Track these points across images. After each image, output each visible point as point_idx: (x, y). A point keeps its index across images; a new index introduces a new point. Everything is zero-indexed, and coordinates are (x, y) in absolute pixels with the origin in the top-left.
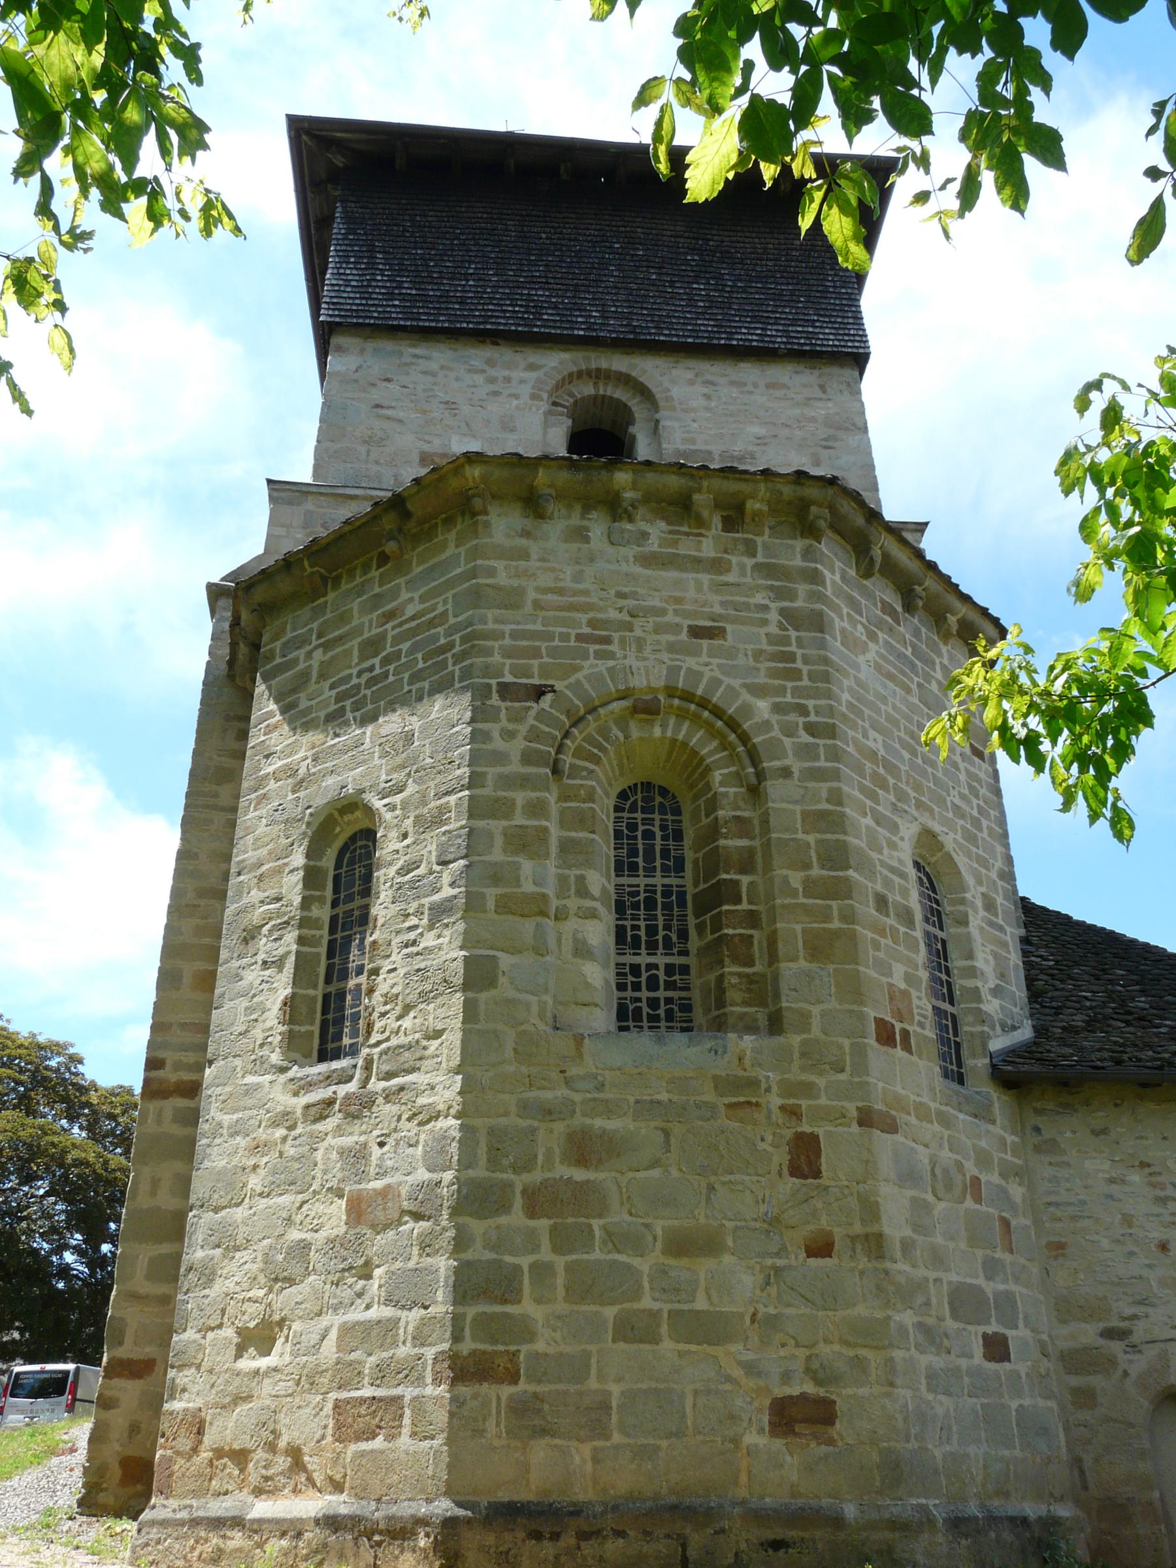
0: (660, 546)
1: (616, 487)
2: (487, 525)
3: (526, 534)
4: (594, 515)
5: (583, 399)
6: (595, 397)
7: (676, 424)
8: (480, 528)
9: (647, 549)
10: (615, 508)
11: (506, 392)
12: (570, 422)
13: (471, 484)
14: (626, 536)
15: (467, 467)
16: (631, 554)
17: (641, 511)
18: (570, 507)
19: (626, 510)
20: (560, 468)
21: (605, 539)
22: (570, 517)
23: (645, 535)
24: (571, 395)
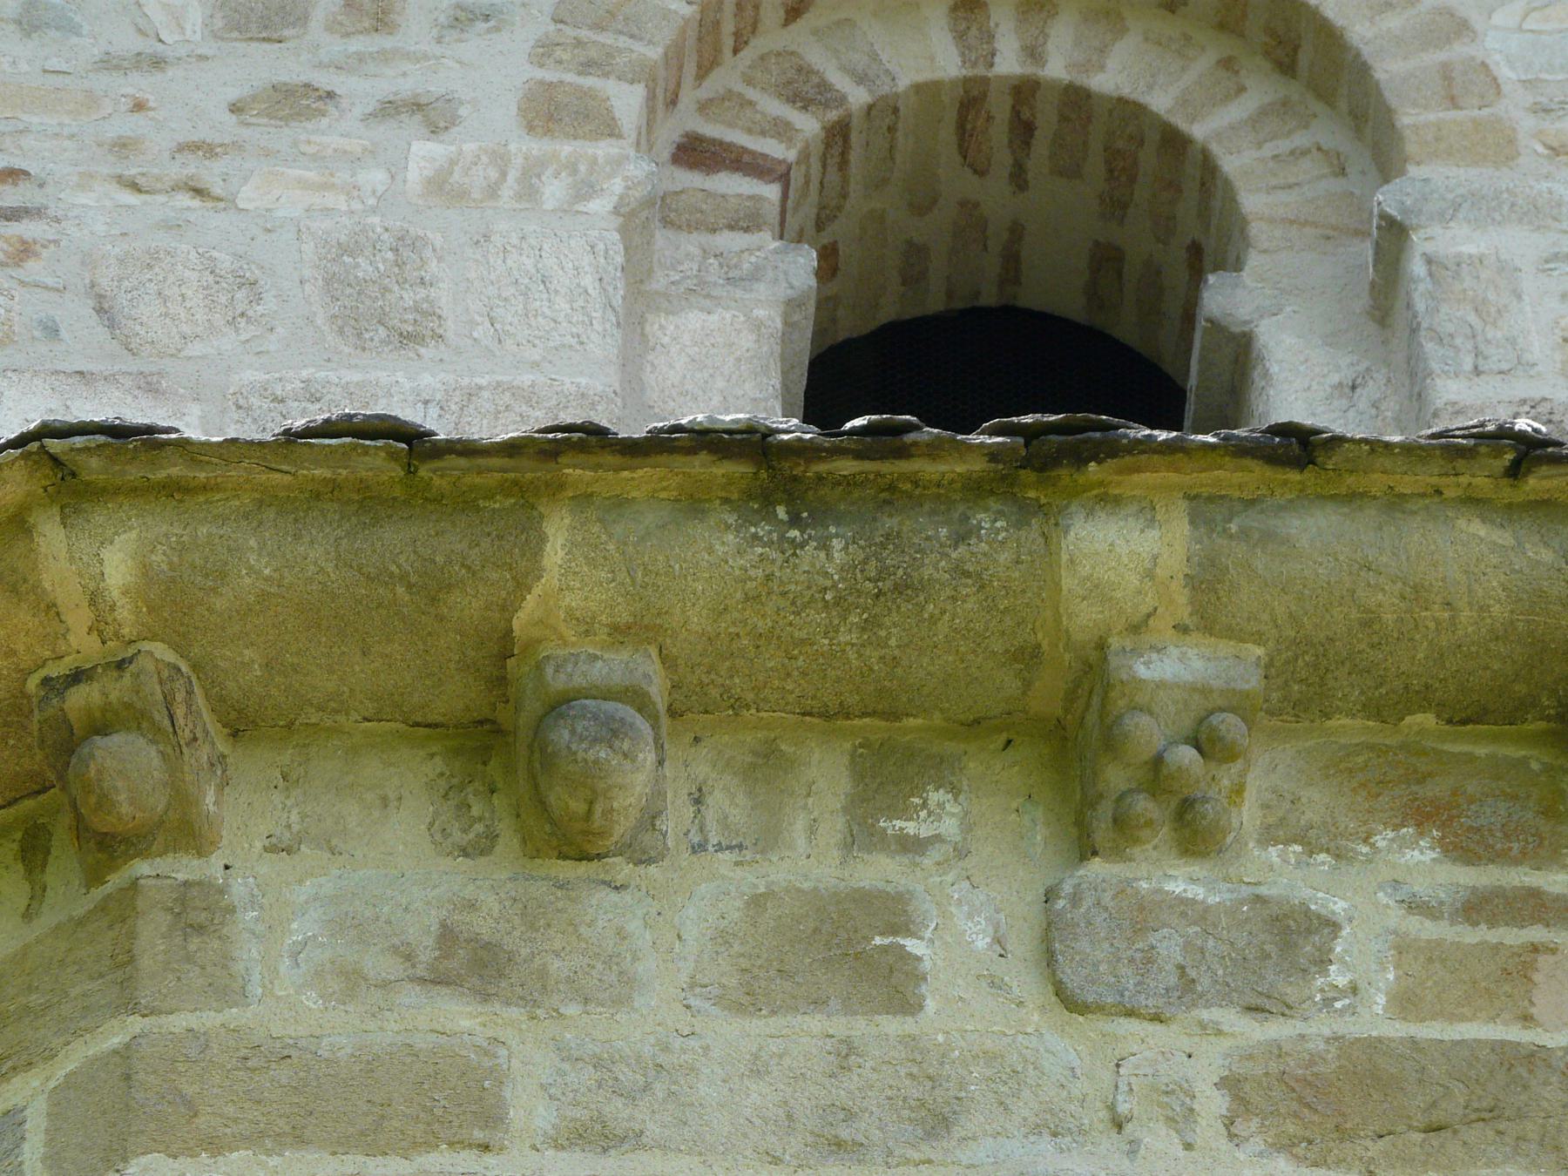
0: (1405, 1003)
1: (1084, 618)
2: (200, 914)
3: (471, 963)
4: (940, 815)
5: (885, 111)
6: (971, 99)
7: (1518, 244)
8: (152, 935)
9: (1320, 1027)
10: (1079, 755)
11: (360, 91)
12: (801, 266)
13: (82, 645)
14: (1169, 946)
15: (51, 535)
16: (1203, 1072)
17: (1262, 780)
18: (767, 767)
19: (1156, 772)
20: (693, 504)
21: (1025, 982)
22: (768, 840)
23: (1297, 936)
24: (805, 90)
